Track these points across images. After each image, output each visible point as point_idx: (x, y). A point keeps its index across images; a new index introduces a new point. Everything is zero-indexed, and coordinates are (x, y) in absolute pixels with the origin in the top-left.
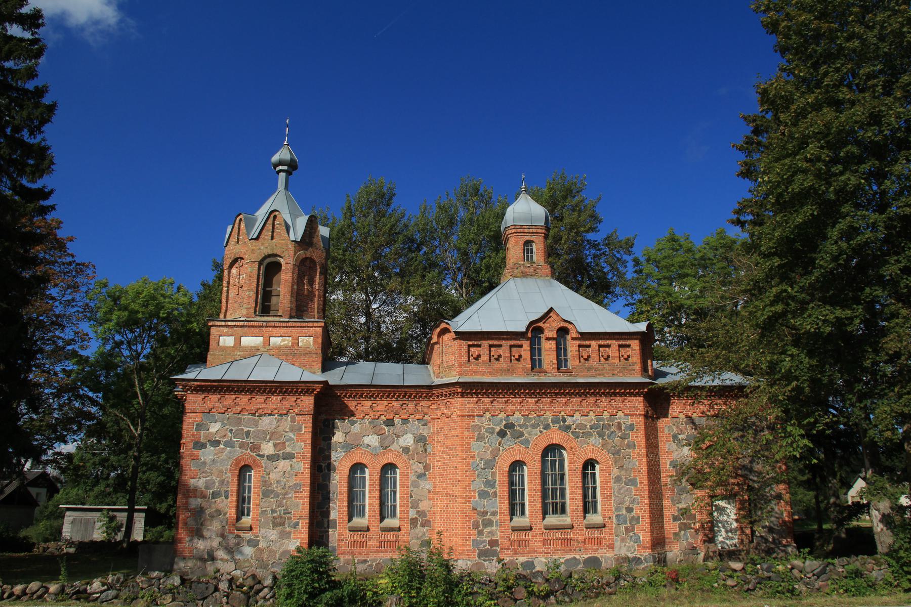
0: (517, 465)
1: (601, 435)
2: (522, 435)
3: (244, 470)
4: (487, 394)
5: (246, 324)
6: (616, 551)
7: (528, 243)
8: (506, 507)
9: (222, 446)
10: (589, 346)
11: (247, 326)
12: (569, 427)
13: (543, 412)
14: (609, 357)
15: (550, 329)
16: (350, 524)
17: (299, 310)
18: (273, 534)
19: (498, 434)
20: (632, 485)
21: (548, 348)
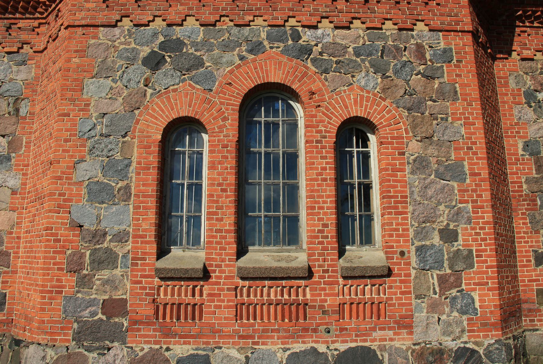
1: (379, 69)
2: (200, 63)
12: (306, 51)
19: (146, 62)
20: (453, 178)
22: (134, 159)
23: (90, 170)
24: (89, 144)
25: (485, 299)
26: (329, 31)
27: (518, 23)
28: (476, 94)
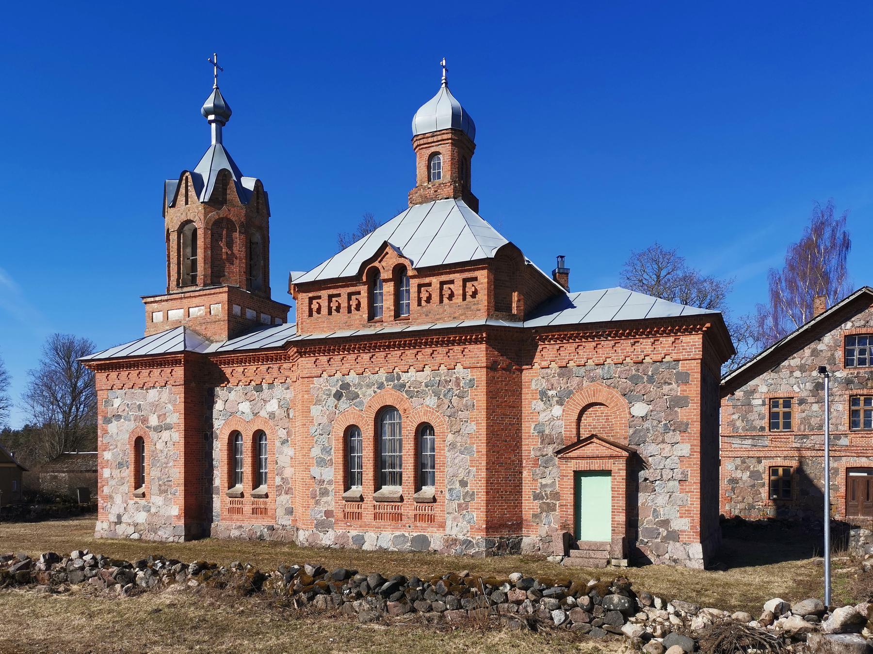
0: (351, 431)
1: (437, 394)
2: (357, 396)
4: (364, 349)
6: (448, 532)
12: (404, 386)
23: (316, 452)
24: (315, 439)
26: (414, 373)
27: (540, 343)
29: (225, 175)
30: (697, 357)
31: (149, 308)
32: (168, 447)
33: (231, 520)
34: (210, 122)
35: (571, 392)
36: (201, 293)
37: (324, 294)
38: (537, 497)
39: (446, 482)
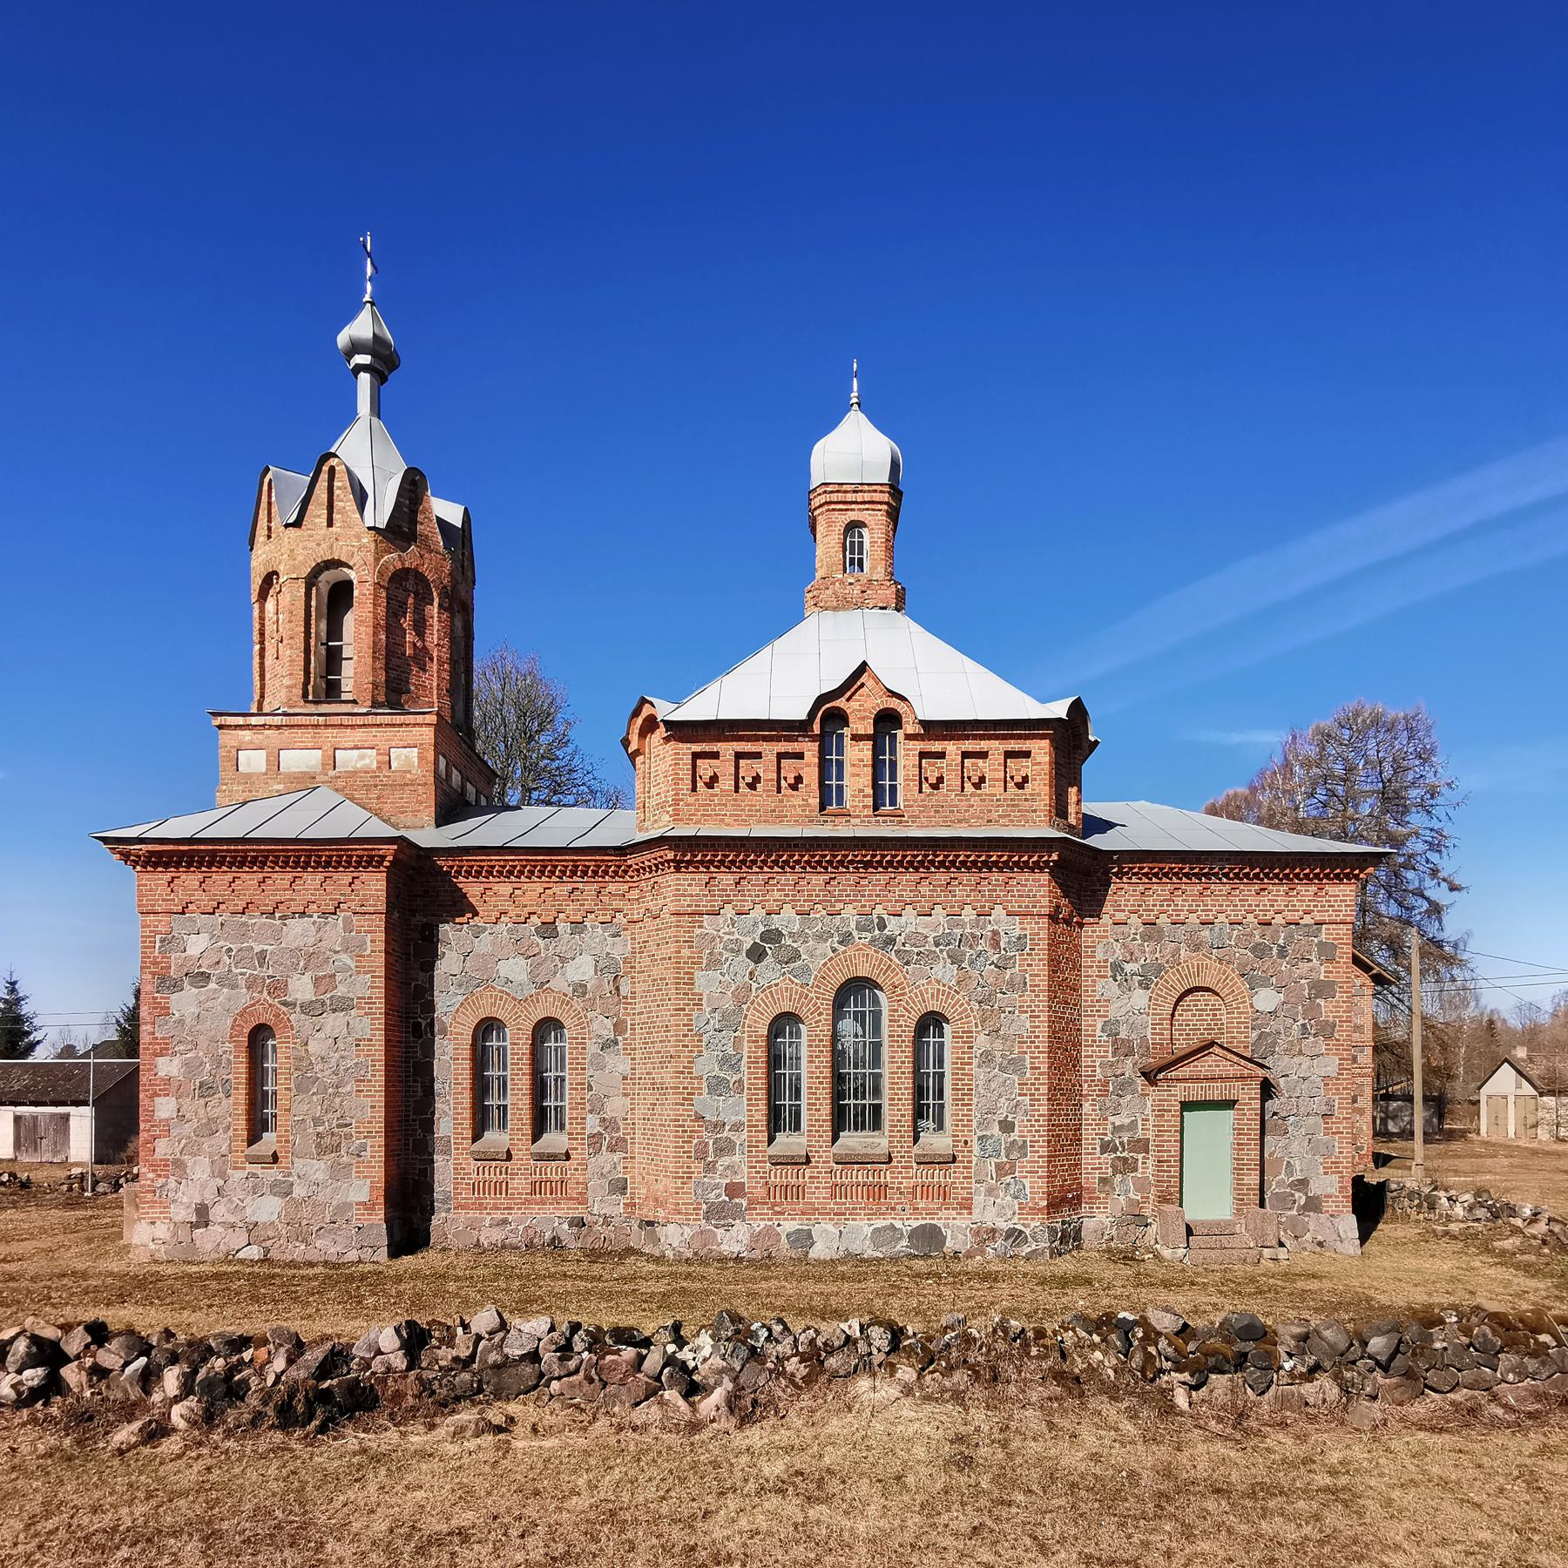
0: (784, 1023)
1: (956, 959)
2: (796, 956)
3: (258, 1038)
4: (814, 866)
5: (285, 720)
6: (975, 1217)
7: (853, 527)
8: (760, 1114)
9: (212, 985)
10: (941, 755)
11: (289, 722)
12: (891, 941)
13: (839, 906)
14: (982, 779)
15: (861, 712)
16: (478, 1146)
17: (394, 692)
18: (317, 1169)
19: (749, 954)
20: (1014, 1072)
21: (857, 756)
22: (745, 1054)
23: (707, 1065)
25: (1034, 1186)
26: (912, 919)
28: (1044, 985)
29: (414, 483)
30: (1348, 919)
31: (226, 738)
32: (342, 1048)
33: (481, 1207)
34: (359, 368)
35: (1160, 968)
36: (370, 720)
37: (727, 749)
38: (1106, 1147)
39: (974, 1123)
